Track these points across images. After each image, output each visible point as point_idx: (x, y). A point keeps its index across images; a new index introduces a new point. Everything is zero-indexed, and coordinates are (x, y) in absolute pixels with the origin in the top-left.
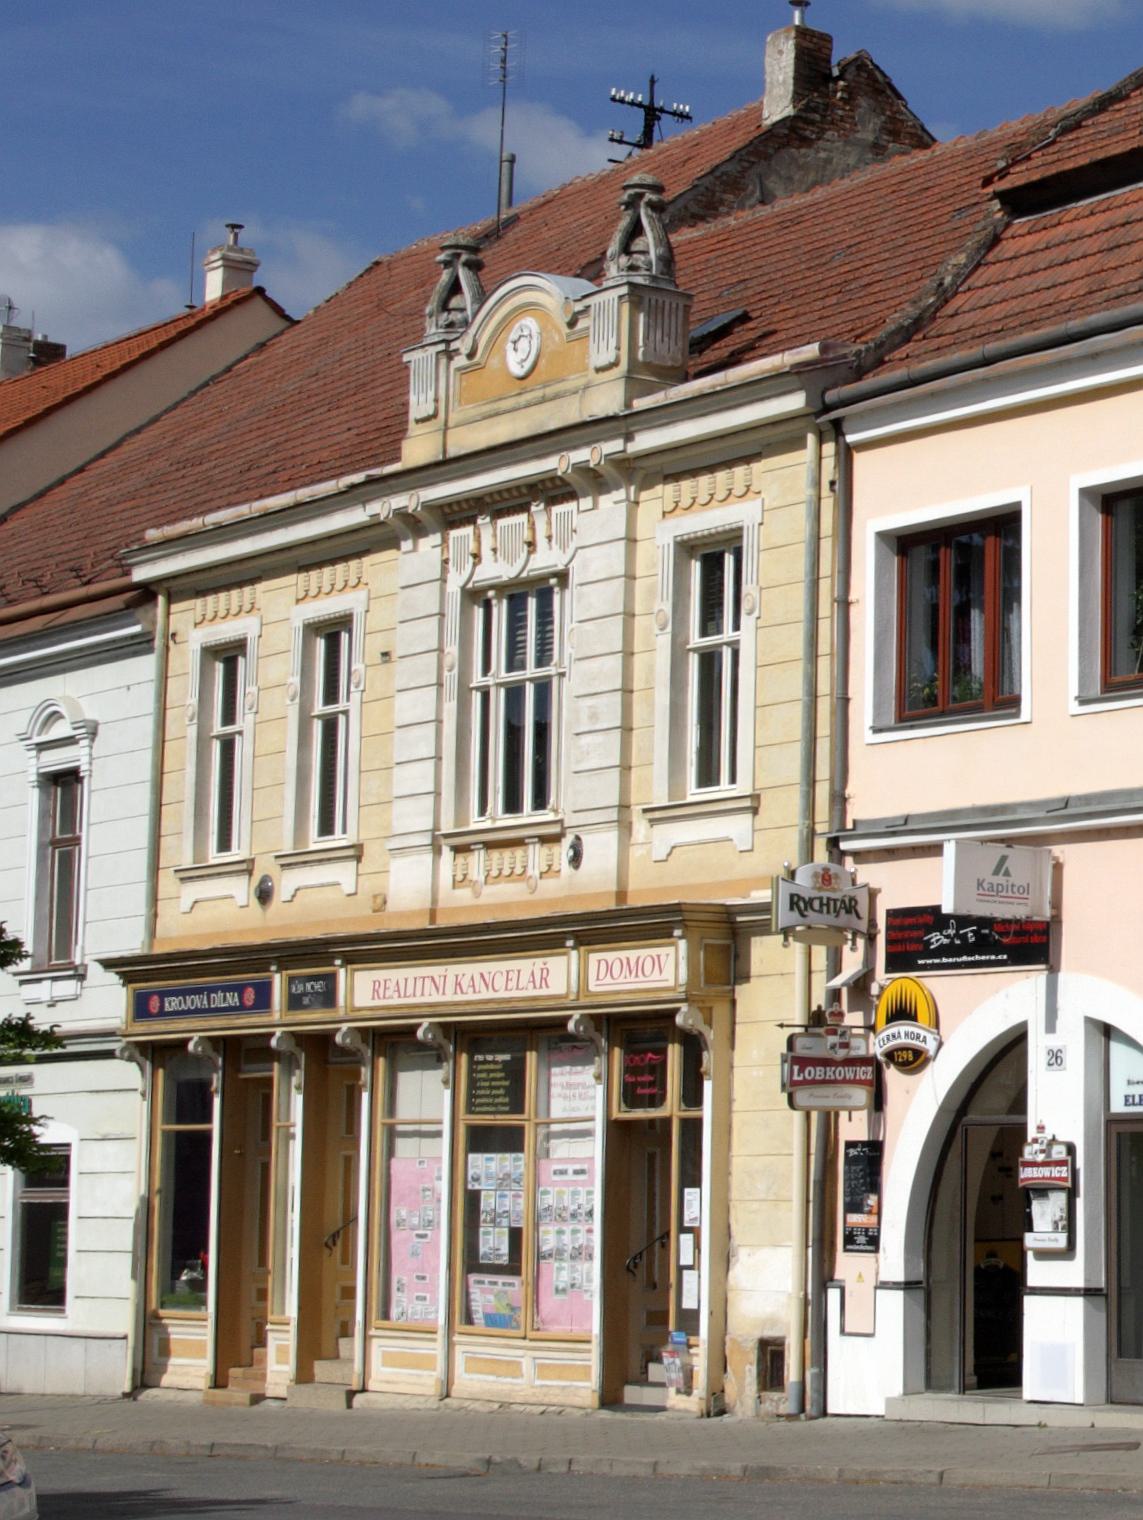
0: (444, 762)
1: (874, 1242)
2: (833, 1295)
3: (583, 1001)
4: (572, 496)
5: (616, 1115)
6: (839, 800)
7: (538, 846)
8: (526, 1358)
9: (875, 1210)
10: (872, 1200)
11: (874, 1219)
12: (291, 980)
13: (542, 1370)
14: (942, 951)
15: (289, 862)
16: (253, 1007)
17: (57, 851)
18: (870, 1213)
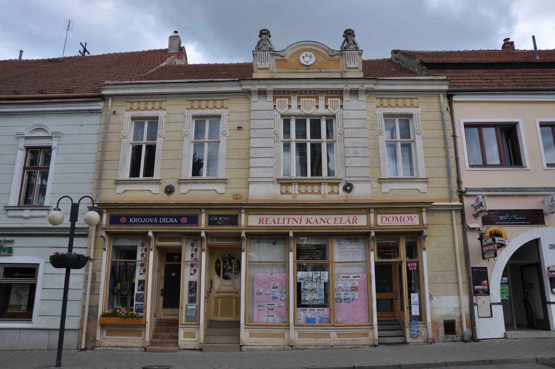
0: (127, 189)
1: (487, 293)
2: (475, 307)
3: (375, 228)
4: (196, 136)
5: (376, 260)
6: (459, 182)
7: (326, 186)
8: (333, 334)
9: (486, 284)
10: (485, 282)
11: (486, 287)
12: (210, 216)
13: (339, 335)
14: (504, 220)
15: (182, 182)
16: (186, 223)
17: (26, 172)
18: (484, 285)
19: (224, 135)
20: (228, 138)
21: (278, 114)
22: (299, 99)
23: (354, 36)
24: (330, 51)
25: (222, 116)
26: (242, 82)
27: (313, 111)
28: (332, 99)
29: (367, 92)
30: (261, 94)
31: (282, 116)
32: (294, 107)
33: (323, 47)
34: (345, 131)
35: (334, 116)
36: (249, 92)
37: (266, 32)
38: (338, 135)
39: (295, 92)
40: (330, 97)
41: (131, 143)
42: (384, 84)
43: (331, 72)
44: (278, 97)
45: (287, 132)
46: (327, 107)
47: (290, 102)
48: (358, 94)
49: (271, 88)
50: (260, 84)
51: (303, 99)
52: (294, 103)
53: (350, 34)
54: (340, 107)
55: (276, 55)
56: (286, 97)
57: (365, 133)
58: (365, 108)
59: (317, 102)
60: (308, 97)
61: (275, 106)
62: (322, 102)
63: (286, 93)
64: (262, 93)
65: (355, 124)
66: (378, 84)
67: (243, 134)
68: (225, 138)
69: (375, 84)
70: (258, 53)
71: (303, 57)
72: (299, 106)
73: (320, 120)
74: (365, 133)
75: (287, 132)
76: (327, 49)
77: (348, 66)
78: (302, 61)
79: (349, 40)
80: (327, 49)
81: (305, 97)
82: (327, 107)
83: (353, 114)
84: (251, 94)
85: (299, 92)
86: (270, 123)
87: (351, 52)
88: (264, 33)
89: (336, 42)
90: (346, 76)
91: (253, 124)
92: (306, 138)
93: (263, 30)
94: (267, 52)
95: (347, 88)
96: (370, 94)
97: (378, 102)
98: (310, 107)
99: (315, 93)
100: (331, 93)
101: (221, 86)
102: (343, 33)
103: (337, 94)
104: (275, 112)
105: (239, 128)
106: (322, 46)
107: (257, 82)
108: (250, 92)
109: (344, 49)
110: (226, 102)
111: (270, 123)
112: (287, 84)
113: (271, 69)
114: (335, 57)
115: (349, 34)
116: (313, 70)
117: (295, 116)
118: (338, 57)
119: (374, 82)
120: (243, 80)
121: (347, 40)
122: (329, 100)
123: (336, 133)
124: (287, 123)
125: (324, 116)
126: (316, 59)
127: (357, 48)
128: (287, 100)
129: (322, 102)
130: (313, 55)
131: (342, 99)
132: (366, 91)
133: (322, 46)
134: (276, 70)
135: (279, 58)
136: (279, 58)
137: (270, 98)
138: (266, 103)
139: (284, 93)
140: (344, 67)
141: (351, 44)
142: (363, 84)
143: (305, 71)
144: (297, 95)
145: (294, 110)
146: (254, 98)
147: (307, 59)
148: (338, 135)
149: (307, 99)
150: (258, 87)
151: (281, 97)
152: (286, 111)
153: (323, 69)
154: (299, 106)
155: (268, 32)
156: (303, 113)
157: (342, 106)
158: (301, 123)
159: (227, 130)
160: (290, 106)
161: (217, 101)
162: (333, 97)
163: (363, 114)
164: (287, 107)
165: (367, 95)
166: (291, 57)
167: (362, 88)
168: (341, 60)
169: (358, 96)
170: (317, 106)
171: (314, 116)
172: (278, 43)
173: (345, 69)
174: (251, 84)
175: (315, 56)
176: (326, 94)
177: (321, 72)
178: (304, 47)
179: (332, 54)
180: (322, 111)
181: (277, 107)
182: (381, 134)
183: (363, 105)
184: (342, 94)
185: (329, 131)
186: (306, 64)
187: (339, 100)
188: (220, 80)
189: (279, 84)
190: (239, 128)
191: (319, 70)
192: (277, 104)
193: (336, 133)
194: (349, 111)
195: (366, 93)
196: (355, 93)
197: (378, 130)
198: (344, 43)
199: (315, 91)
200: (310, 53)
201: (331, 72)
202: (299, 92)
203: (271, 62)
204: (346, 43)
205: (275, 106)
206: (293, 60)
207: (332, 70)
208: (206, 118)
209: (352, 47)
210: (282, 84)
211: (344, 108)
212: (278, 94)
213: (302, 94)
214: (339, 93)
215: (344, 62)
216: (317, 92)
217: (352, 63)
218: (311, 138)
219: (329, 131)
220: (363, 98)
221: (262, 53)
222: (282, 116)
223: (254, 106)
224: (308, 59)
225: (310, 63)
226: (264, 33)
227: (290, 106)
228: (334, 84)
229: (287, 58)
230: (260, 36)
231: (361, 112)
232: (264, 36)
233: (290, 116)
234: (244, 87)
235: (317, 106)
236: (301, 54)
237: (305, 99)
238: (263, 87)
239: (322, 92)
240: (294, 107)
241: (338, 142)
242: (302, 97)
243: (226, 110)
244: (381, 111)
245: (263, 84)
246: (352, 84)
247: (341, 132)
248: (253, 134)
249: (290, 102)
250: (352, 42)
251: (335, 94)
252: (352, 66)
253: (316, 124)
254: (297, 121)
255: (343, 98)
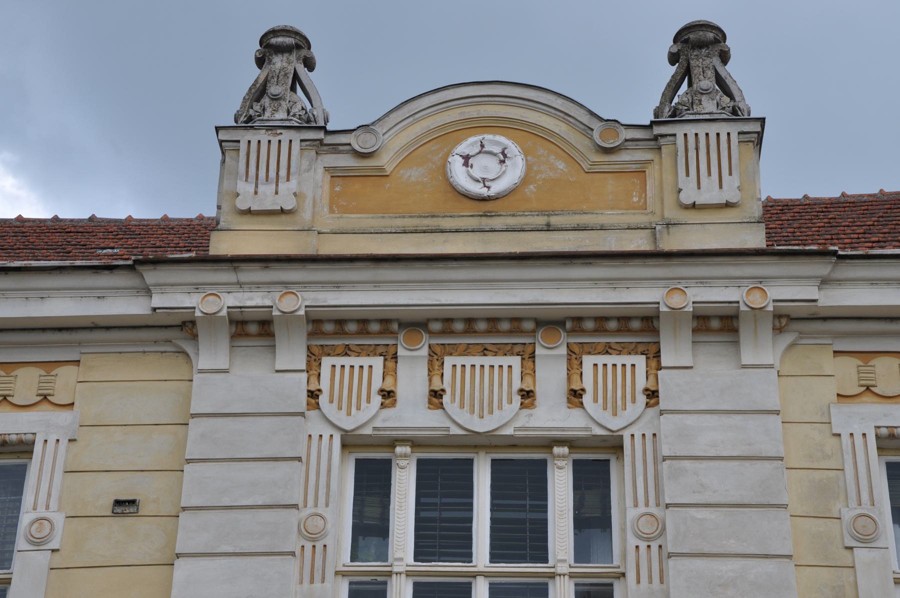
19: (37, 543)
20: (58, 561)
21: (327, 432)
22: (435, 359)
23: (725, 57)
24: (596, 125)
25: (38, 448)
26: (152, 276)
27: (505, 418)
28: (601, 359)
29: (785, 320)
30: (709, 330)
31: (349, 442)
32: (409, 399)
33: (565, 107)
34: (671, 518)
35: (615, 445)
36: (187, 326)
37: (711, 35)
38: (632, 541)
39: (415, 324)
40: (592, 350)
41: (344, 574)
42: (873, 282)
43: (602, 228)
44: (330, 352)
45: (371, 528)
46: (575, 396)
47: (389, 371)
48: (735, 331)
49: (296, 303)
50: (240, 284)
51: (459, 361)
52: (412, 378)
53: (701, 45)
54: (642, 399)
55: (335, 148)
56: (372, 351)
57: (776, 531)
58: (773, 403)
59: (529, 371)
60: (485, 351)
61: (313, 395)
62: (551, 373)
63: (375, 327)
64: (253, 330)
65: (723, 482)
66: (840, 282)
67: (139, 538)
68: (42, 558)
69: (824, 282)
70: (244, 136)
71: (466, 159)
72: (436, 395)
73: (543, 463)
74: (776, 531)
75: (371, 528)
76: (585, 118)
77: (687, 198)
78: (460, 176)
79: (695, 71)
80: (585, 118)
81: (467, 351)
82: (575, 396)
83: (712, 435)
84: (195, 337)
85: (436, 326)
86: (283, 482)
87: (701, 129)
88: (284, 47)
89: (637, 90)
90: (673, 242)
91: (198, 485)
92: (467, 557)
93: (274, 32)
94: (286, 135)
95: (676, 301)
96: (802, 334)
97: (847, 373)
98: (487, 399)
99: (516, 331)
100: (600, 330)
101: (43, 295)
102: (667, 44)
103: (630, 331)
104: (315, 425)
105: (124, 506)
106: (558, 103)
107: (225, 276)
108: (193, 323)
109: (671, 114)
110: (66, 376)
111: (283, 482)
112: (377, 284)
113: (306, 215)
114: (625, 156)
115: (698, 45)
116: (511, 221)
117: (416, 444)
118: (648, 156)
119: (822, 268)
120: (157, 262)
121: (687, 73)
122: (588, 361)
123: (623, 530)
124: (373, 481)
125: (560, 442)
126: (529, 167)
127: (734, 112)
128: (378, 363)
129: (551, 373)
130: (513, 149)
131: (654, 355)
132: (777, 316)
133: (558, 103)
134: (327, 221)
135: (345, 161)
136: (345, 161)
137: (292, 354)
138: (274, 377)
139: (363, 332)
140: (669, 199)
141: (705, 92)
142: (761, 279)
143: (473, 223)
144: (564, 338)
145: (413, 415)
146: (211, 355)
147: (484, 166)
148: (632, 541)
149: (478, 360)
150: (231, 300)
151: (347, 352)
152: (367, 416)
153: (562, 212)
154: (436, 395)
155: (720, 35)
156: (599, 431)
157: (652, 395)
158: (444, 482)
159: (59, 519)
160: (388, 395)
161: (21, 372)
162: (607, 350)
163: (764, 435)
164: (377, 400)
165: (787, 339)
166: (409, 157)
167: (756, 301)
168: (652, 173)
169: (736, 343)
170: (527, 395)
171: (513, 444)
172: (341, 94)
173: (672, 213)
174: (197, 287)
175: (526, 153)
176: (572, 332)
177: (549, 228)
178: (472, 112)
179: (613, 145)
180: (551, 416)
181: (323, 399)
182: (867, 539)
183: (764, 390)
184: (656, 332)
185: (593, 520)
186: (477, 189)
187: (640, 361)
188: (34, 263)
189: (337, 286)
190: (124, 506)
191: (541, 221)
192: (325, 385)
193: (623, 530)
194: (690, 420)
195: (778, 330)
196: (719, 326)
197: (848, 515)
198: (673, 87)
199: (516, 320)
200: (496, 141)
201: (602, 228)
202: (436, 326)
203: (306, 182)
204: (684, 87)
205: (313, 395)
206: (414, 174)
207: (609, 217)
208: (477, 447)
209: (709, 106)
210: (352, 285)
211: (663, 405)
212: (330, 332)
213: (450, 333)
214: (640, 329)
215: (668, 178)
216: (529, 326)
217: (709, 183)
218: (495, 557)
219: (593, 520)
220: (761, 349)
221: (263, 136)
222: (349, 442)
223: (207, 394)
224: (490, 167)
225: (497, 188)
226: (284, 47)
227: (388, 395)
228: (612, 283)
229: (386, 160)
230: (260, 62)
231: (753, 422)
232: (279, 62)
233: (392, 443)
234: (158, 301)
235: (527, 395)
236: (458, 142)
237: (468, 361)
238: (255, 299)
239: (552, 322)
240: (409, 399)
241: (631, 576)
242: (452, 350)
243: (64, 417)
244: (865, 420)
245: (258, 285)
246: (702, 281)
247: (647, 528)
248: (192, 533)
249: (389, 371)
250: (707, 83)
251: (618, 331)
252: (710, 194)
253: (521, 482)
254: (579, 467)
255: (657, 355)
